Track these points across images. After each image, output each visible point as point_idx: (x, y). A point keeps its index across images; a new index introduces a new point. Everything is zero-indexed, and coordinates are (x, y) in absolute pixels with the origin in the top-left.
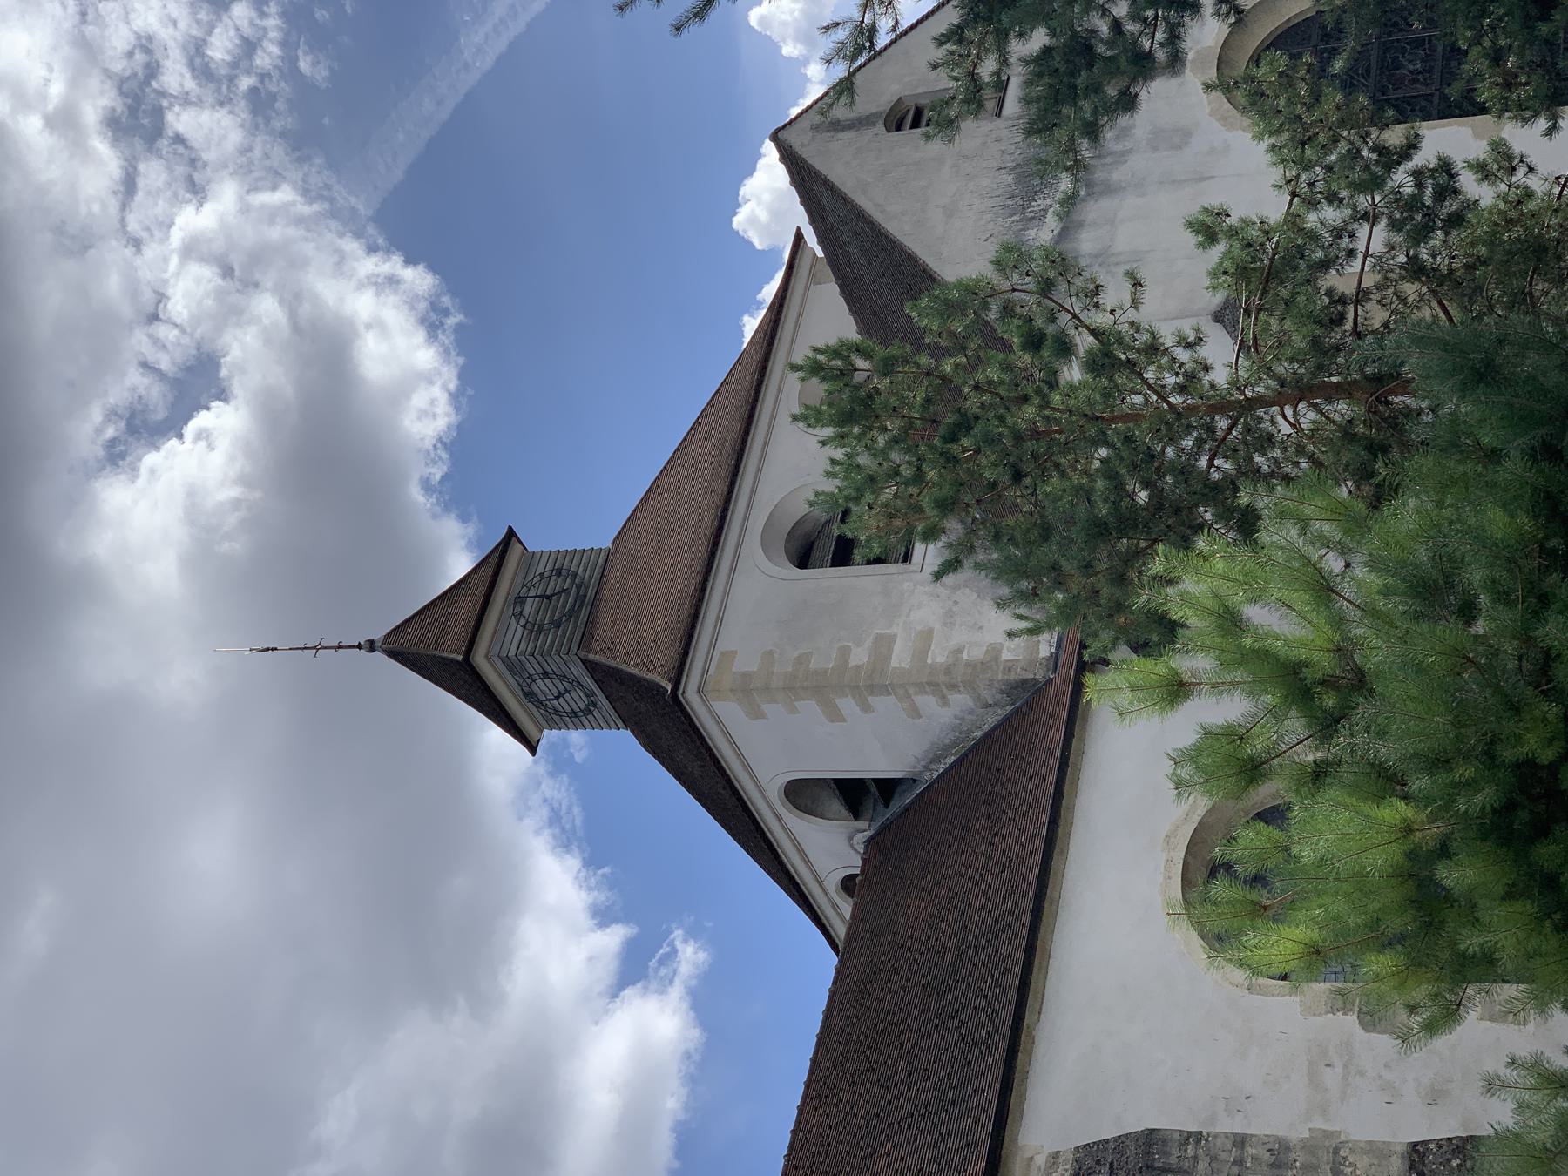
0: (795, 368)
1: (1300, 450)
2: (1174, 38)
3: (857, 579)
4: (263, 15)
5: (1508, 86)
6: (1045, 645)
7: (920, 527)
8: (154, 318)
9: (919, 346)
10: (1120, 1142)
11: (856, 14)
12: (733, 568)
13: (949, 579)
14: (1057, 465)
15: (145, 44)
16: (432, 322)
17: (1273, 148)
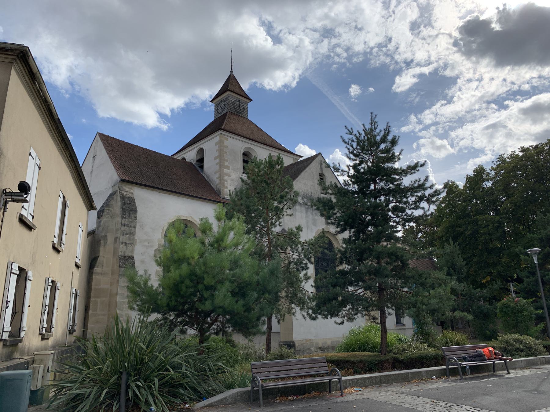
0: (279, 154)
1: (260, 242)
2: (332, 223)
3: (240, 164)
4: (344, 59)
5: (320, 280)
6: (227, 197)
7: (250, 176)
8: (290, 33)
9: (282, 177)
10: (135, 206)
11: (341, 169)
12: (243, 141)
13: (240, 180)
14: (259, 200)
15: (340, 35)
16: (286, 86)
17: (312, 240)
